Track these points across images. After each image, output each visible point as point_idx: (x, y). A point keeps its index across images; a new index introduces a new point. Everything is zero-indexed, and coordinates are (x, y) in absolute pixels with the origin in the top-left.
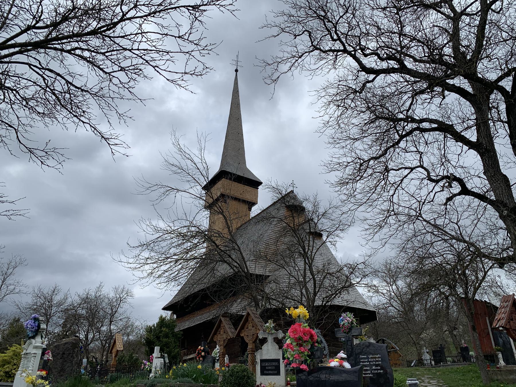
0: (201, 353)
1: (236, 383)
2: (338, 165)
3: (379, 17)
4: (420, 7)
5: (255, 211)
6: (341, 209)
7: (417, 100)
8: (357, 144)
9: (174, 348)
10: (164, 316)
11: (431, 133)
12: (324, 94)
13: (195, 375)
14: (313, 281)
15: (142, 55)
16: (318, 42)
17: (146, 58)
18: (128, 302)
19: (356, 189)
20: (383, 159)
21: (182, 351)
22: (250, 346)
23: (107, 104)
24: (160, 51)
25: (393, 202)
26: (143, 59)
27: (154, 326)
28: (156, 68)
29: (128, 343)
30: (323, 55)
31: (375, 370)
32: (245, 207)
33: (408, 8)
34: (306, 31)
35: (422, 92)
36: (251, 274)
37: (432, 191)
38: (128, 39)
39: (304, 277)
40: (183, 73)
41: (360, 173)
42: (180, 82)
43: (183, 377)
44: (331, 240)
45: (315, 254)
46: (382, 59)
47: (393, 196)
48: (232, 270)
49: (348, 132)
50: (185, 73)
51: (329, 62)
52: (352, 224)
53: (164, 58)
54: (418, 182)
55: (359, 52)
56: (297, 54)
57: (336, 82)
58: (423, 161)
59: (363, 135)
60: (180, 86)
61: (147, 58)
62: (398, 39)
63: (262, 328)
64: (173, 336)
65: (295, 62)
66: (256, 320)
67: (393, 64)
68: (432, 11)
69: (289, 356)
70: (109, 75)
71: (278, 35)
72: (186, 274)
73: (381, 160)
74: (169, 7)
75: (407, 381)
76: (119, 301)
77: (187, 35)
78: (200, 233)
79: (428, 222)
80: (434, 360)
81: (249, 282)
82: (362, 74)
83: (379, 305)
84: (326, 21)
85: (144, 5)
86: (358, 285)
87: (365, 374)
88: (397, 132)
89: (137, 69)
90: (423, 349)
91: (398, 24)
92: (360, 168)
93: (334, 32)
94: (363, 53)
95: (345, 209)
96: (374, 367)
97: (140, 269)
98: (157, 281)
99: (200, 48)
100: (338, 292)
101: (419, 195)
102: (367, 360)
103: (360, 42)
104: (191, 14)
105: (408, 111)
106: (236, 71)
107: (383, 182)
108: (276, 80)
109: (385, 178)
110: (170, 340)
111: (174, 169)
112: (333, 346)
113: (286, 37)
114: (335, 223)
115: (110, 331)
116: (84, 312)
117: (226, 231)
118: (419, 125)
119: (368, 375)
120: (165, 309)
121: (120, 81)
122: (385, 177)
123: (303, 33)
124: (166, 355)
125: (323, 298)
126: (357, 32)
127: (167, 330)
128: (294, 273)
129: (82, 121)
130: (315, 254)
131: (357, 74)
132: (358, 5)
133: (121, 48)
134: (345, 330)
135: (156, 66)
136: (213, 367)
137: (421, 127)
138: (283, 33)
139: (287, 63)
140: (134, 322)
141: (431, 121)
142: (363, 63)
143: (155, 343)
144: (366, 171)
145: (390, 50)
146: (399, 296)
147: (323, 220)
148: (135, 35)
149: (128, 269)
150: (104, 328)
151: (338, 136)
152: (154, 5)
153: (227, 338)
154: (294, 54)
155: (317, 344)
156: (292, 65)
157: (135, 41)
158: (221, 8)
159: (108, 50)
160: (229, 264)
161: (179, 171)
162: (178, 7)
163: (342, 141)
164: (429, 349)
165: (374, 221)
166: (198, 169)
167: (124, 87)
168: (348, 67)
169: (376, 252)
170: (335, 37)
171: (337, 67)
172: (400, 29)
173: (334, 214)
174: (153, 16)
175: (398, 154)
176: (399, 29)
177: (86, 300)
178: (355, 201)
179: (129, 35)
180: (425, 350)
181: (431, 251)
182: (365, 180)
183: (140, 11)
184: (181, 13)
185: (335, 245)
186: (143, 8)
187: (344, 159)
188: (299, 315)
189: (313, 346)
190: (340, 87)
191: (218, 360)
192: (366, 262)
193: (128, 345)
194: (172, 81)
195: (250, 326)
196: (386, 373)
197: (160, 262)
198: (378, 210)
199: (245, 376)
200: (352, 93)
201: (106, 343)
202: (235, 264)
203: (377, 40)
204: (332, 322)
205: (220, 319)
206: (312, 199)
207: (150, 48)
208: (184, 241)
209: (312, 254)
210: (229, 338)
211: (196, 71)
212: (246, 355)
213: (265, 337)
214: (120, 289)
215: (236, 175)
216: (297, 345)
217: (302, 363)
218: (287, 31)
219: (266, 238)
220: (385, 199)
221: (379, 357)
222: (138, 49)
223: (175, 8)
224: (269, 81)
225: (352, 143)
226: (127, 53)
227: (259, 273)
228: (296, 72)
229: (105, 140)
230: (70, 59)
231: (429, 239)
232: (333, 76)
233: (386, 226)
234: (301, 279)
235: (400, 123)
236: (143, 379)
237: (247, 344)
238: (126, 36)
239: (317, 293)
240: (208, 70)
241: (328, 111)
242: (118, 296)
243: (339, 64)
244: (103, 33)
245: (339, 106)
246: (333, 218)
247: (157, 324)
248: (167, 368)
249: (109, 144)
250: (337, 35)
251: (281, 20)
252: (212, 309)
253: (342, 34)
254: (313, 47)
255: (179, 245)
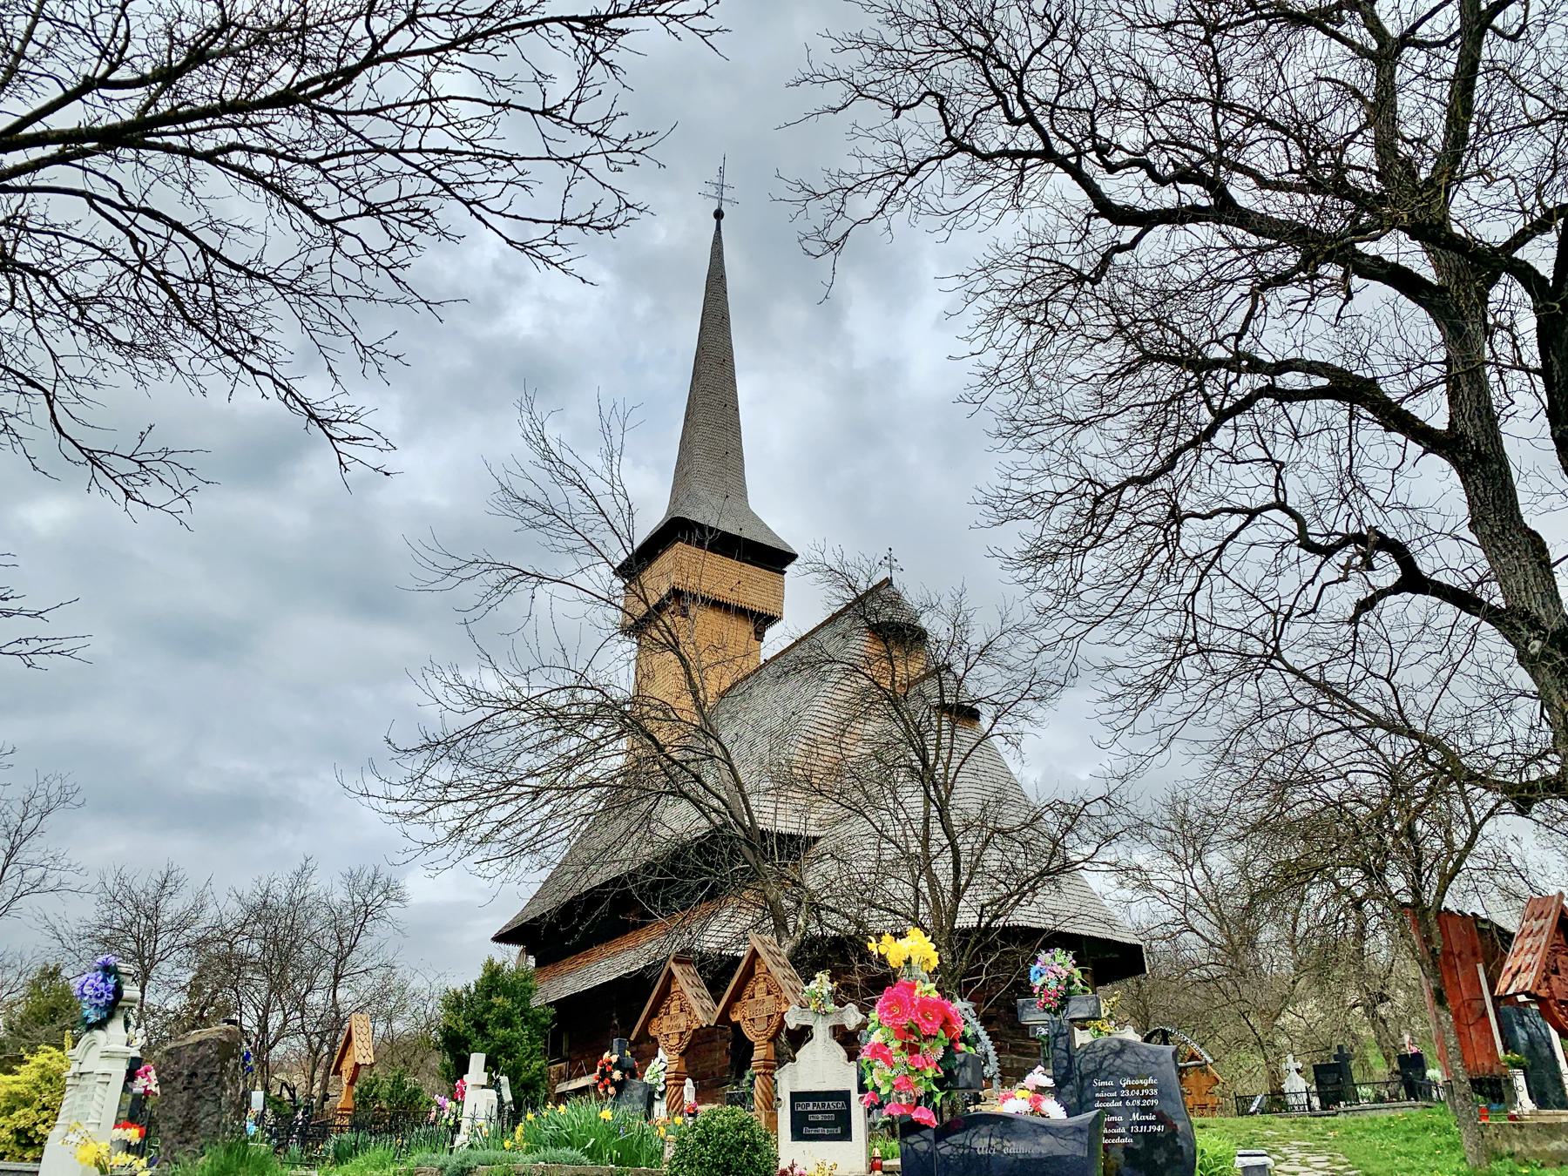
0: (611, 1073)
1: (719, 1165)
2: (1028, 502)
3: (1151, 52)
4: (1276, 22)
5: (776, 639)
6: (1037, 635)
7: (1266, 304)
8: (1086, 437)
9: (528, 1057)
10: (498, 961)
11: (1311, 404)
12: (983, 285)
13: (592, 1140)
14: (950, 854)
15: (431, 166)
16: (967, 128)
17: (444, 175)
18: (388, 919)
19: (1081, 575)
20: (1163, 484)
21: (552, 1067)
22: (759, 1054)
23: (326, 315)
24: (487, 156)
25: (1194, 614)
26: (434, 179)
27: (467, 990)
28: (473, 207)
29: (388, 1041)
30: (981, 166)
31: (1140, 1123)
32: (745, 629)
33: (1238, 23)
34: (930, 93)
35: (1283, 280)
36: (762, 832)
37: (1312, 581)
38: (389, 118)
39: (925, 841)
40: (555, 222)
41: (1093, 526)
42: (546, 250)
43: (556, 1147)
44: (1006, 729)
45: (958, 771)
46: (1161, 181)
47: (1193, 594)
48: (704, 821)
49: (1059, 400)
50: (564, 222)
51: (1001, 188)
52: (1070, 682)
53: (499, 175)
54: (1269, 554)
55: (1090, 164)
56: (903, 163)
57: (1020, 249)
58: (1284, 490)
59: (1104, 410)
60: (547, 260)
61: (446, 176)
62: (1209, 118)
63: (797, 997)
64: (526, 1022)
65: (897, 188)
66: (778, 972)
67: (1194, 194)
68: (1312, 34)
69: (879, 1083)
70: (332, 227)
71: (845, 106)
72: (566, 833)
73: (1159, 487)
74: (513, 21)
75: (1237, 1158)
76: (363, 915)
77: (569, 105)
78: (607, 708)
79: (1300, 675)
80: (1319, 1094)
81: (755, 856)
82: (1101, 226)
83: (1151, 926)
84: (990, 62)
85: (437, 15)
86: (1087, 865)
87: (1107, 1136)
88: (1208, 400)
89: (417, 210)
90: (1286, 1062)
91: (1209, 74)
92: (1093, 510)
93: (1014, 97)
94: (1103, 160)
95: (1048, 635)
96: (1136, 1117)
97: (425, 818)
98: (478, 855)
99: (608, 146)
100: (1026, 887)
101: (1274, 594)
102: (1115, 1094)
103: (1094, 129)
104: (580, 43)
105: (1239, 336)
106: (719, 215)
107: (1164, 554)
108: (837, 244)
109: (1173, 542)
110: (516, 1035)
111: (530, 512)
112: (1012, 1052)
113: (869, 113)
114: (1018, 676)
115: (335, 1004)
116: (255, 947)
117: (687, 701)
118: (1273, 380)
119: (1118, 1140)
120: (501, 938)
121: (364, 246)
122: (1169, 538)
123: (921, 100)
124: (504, 1079)
125: (983, 907)
126: (1085, 97)
127: (508, 1004)
128: (894, 831)
129: (250, 368)
130: (958, 771)
131: (1085, 225)
132: (1087, 15)
133: (368, 146)
134: (1050, 1002)
135: (474, 202)
136: (648, 1115)
137: (1279, 385)
138: (861, 102)
139: (872, 192)
140: (408, 978)
141: (1311, 368)
142: (1103, 190)
143: (470, 1042)
144: (1111, 519)
145: (1186, 151)
146: (1213, 900)
147: (981, 669)
148: (409, 108)
149: (390, 819)
150: (316, 998)
151: (1027, 414)
152: (467, 17)
153: (688, 1028)
154: (894, 164)
155: (962, 1046)
156: (889, 198)
157: (410, 125)
158: (673, 25)
159: (329, 153)
160: (696, 803)
161: (545, 519)
162: (542, 22)
163: (1040, 428)
164: (1303, 1062)
165: (1136, 670)
166: (602, 513)
167: (378, 264)
168: (1059, 205)
169: (1143, 766)
170: (1019, 113)
171: (1023, 203)
172: (1215, 87)
173: (1014, 651)
174: (466, 50)
175: (1211, 467)
176: (1211, 90)
177: (261, 912)
178: (1078, 611)
179: (393, 107)
180: (1290, 1063)
181: (1311, 762)
182: (1110, 546)
183: (426, 33)
184: (551, 39)
185: (1017, 745)
186: (434, 23)
187: (1047, 484)
188: (910, 958)
189: (949, 1050)
190: (1032, 263)
191: (662, 1094)
192: (1112, 797)
193: (391, 1048)
194: (524, 247)
195: (759, 989)
196: (1173, 1133)
197: (486, 795)
198: (1149, 639)
199: (744, 1144)
200: (1069, 282)
201: (322, 1041)
202: (715, 803)
203: (1146, 121)
204: (1010, 977)
205: (670, 969)
206: (947, 606)
207: (455, 146)
208: (560, 733)
209: (947, 771)
210: (696, 1026)
211: (596, 217)
212: (748, 1077)
213: (804, 1023)
214: (365, 878)
215: (718, 531)
216: (903, 1048)
217: (918, 1104)
218: (872, 94)
219: (810, 723)
220: (1171, 606)
221: (1150, 1086)
222: (420, 150)
223: (533, 24)
224: (816, 248)
225: (1069, 435)
226: (387, 162)
227: (789, 831)
228: (899, 218)
229: (321, 426)
230: (212, 179)
231: (1305, 727)
232: (1011, 231)
233: (1173, 686)
234: (915, 847)
235: (1214, 373)
236: (435, 1152)
237: (750, 1047)
238: (384, 109)
239: (964, 891)
240: (632, 213)
241: (995, 337)
242: (358, 899)
243: (1031, 194)
244: (314, 101)
245: (1029, 322)
246: (1011, 661)
247: (477, 985)
248: (510, 1116)
249: (331, 438)
250: (1025, 105)
251: (852, 60)
252: (643, 939)
253: (1041, 103)
254: (950, 143)
255: (544, 745)
